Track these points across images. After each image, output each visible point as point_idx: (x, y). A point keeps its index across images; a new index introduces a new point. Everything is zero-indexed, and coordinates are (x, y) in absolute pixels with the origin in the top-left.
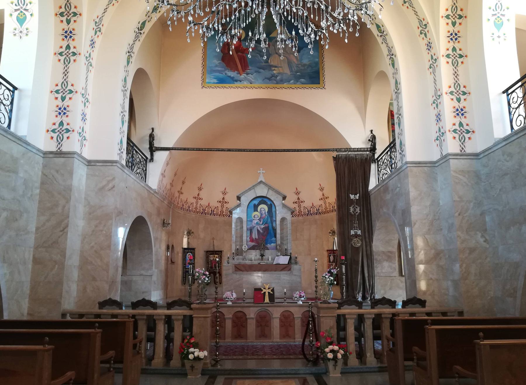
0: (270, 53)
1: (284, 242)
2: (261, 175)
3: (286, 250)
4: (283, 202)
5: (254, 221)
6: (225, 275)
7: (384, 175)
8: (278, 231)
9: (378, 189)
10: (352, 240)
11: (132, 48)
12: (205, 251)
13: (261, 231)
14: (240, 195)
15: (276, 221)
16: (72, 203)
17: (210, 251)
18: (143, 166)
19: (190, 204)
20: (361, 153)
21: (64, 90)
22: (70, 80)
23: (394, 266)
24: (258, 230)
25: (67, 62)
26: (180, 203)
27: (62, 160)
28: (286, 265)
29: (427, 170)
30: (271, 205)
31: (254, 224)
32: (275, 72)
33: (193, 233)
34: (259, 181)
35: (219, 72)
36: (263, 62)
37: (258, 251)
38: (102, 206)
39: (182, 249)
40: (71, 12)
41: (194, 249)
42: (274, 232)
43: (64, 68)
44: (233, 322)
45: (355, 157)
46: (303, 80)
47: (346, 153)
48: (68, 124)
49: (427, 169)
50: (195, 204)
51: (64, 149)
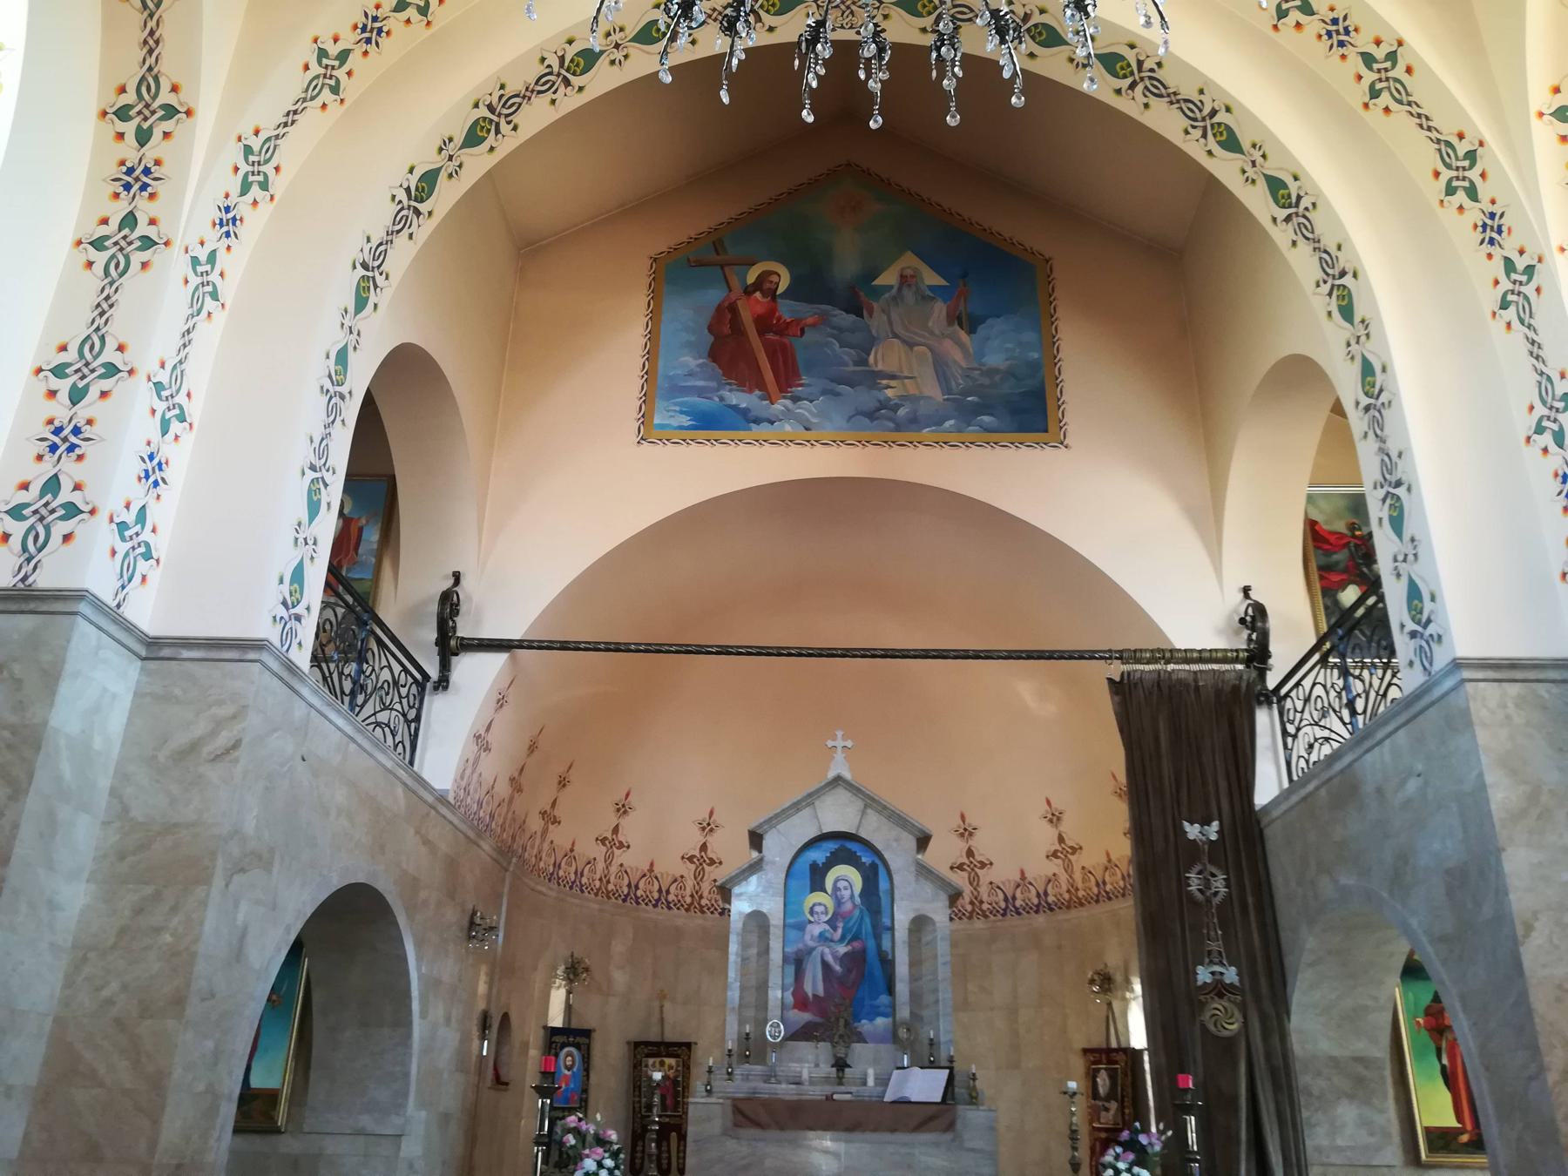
0: (874, 332)
1: (926, 1013)
2: (839, 756)
3: (932, 1043)
4: (920, 856)
5: (809, 927)
6: (695, 1141)
7: (1317, 745)
8: (902, 969)
9: (1304, 799)
10: (1202, 1005)
11: (380, 251)
12: (628, 1043)
13: (838, 968)
14: (760, 826)
15: (892, 929)
16: (32, 803)
17: (647, 1044)
18: (405, 701)
19: (585, 860)
20: (1215, 667)
21: (87, 364)
22: (117, 330)
23: (1379, 1119)
24: (825, 965)
25: (115, 271)
26: (549, 855)
27: (26, 622)
28: (935, 1108)
29: (1546, 696)
30: (874, 867)
32: (889, 393)
33: (587, 970)
34: (831, 775)
35: (700, 392)
36: (851, 363)
37: (824, 1048)
38: (176, 825)
39: (541, 1032)
40: (155, 105)
41: (587, 1033)
43: (103, 290)
45: (1193, 684)
46: (986, 419)
47: (1158, 667)
48: (78, 487)
49: (1548, 692)
50: (601, 865)
51: (44, 580)
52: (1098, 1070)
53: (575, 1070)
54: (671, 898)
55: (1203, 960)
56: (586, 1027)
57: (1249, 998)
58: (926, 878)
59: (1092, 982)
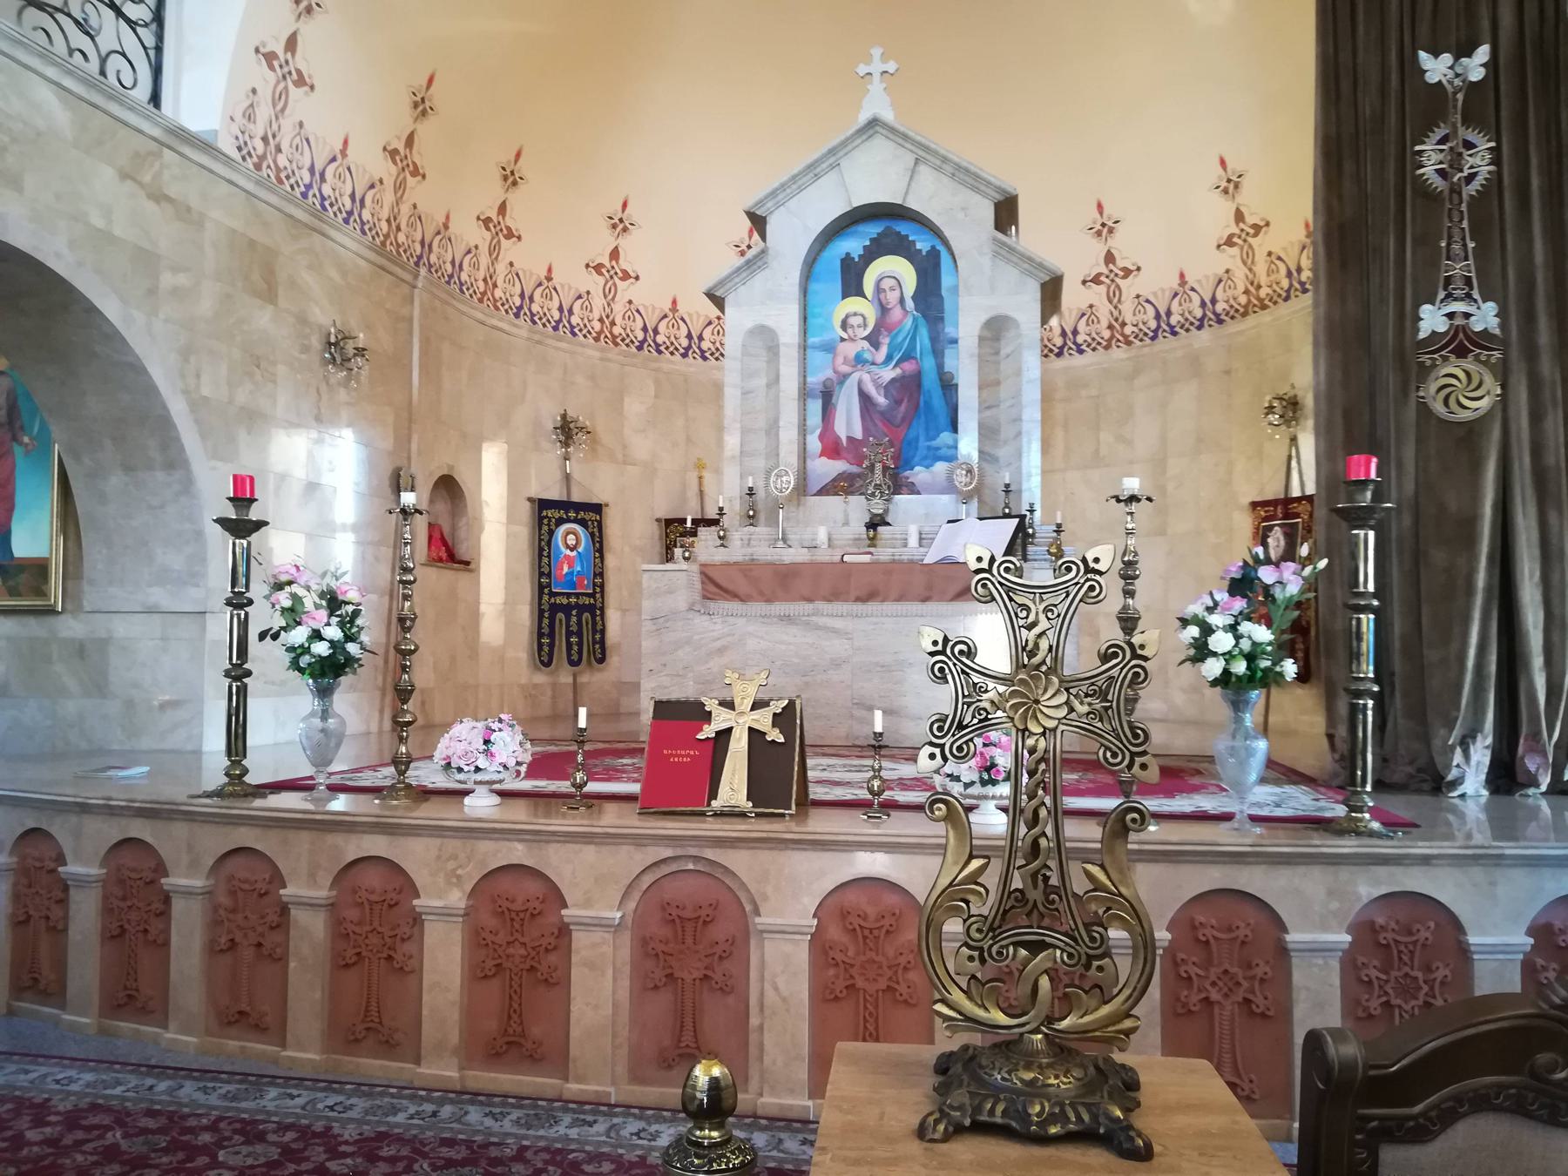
1: (1003, 453)
2: (877, 87)
5: (842, 347)
10: (1425, 372)
13: (881, 400)
14: (761, 202)
26: (411, 225)
31: (846, 361)
34: (863, 117)
41: (597, 508)
42: (947, 403)
44: (477, 940)
50: (598, 302)
52: (1270, 528)
53: (580, 550)
54: (705, 345)
55: (1435, 294)
56: (595, 501)
57: (1515, 353)
58: (1009, 261)
59: (1270, 410)
